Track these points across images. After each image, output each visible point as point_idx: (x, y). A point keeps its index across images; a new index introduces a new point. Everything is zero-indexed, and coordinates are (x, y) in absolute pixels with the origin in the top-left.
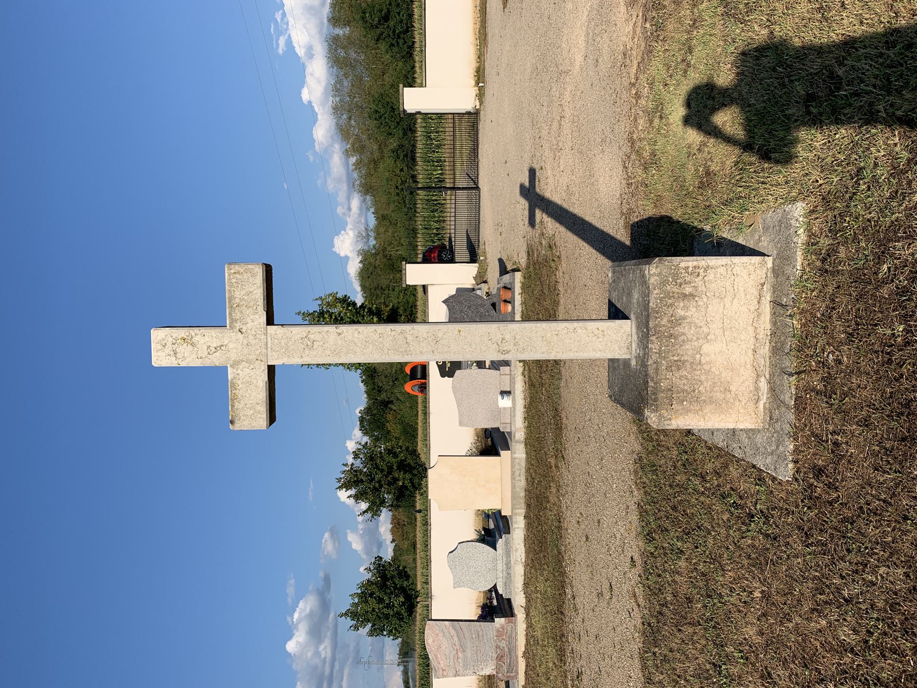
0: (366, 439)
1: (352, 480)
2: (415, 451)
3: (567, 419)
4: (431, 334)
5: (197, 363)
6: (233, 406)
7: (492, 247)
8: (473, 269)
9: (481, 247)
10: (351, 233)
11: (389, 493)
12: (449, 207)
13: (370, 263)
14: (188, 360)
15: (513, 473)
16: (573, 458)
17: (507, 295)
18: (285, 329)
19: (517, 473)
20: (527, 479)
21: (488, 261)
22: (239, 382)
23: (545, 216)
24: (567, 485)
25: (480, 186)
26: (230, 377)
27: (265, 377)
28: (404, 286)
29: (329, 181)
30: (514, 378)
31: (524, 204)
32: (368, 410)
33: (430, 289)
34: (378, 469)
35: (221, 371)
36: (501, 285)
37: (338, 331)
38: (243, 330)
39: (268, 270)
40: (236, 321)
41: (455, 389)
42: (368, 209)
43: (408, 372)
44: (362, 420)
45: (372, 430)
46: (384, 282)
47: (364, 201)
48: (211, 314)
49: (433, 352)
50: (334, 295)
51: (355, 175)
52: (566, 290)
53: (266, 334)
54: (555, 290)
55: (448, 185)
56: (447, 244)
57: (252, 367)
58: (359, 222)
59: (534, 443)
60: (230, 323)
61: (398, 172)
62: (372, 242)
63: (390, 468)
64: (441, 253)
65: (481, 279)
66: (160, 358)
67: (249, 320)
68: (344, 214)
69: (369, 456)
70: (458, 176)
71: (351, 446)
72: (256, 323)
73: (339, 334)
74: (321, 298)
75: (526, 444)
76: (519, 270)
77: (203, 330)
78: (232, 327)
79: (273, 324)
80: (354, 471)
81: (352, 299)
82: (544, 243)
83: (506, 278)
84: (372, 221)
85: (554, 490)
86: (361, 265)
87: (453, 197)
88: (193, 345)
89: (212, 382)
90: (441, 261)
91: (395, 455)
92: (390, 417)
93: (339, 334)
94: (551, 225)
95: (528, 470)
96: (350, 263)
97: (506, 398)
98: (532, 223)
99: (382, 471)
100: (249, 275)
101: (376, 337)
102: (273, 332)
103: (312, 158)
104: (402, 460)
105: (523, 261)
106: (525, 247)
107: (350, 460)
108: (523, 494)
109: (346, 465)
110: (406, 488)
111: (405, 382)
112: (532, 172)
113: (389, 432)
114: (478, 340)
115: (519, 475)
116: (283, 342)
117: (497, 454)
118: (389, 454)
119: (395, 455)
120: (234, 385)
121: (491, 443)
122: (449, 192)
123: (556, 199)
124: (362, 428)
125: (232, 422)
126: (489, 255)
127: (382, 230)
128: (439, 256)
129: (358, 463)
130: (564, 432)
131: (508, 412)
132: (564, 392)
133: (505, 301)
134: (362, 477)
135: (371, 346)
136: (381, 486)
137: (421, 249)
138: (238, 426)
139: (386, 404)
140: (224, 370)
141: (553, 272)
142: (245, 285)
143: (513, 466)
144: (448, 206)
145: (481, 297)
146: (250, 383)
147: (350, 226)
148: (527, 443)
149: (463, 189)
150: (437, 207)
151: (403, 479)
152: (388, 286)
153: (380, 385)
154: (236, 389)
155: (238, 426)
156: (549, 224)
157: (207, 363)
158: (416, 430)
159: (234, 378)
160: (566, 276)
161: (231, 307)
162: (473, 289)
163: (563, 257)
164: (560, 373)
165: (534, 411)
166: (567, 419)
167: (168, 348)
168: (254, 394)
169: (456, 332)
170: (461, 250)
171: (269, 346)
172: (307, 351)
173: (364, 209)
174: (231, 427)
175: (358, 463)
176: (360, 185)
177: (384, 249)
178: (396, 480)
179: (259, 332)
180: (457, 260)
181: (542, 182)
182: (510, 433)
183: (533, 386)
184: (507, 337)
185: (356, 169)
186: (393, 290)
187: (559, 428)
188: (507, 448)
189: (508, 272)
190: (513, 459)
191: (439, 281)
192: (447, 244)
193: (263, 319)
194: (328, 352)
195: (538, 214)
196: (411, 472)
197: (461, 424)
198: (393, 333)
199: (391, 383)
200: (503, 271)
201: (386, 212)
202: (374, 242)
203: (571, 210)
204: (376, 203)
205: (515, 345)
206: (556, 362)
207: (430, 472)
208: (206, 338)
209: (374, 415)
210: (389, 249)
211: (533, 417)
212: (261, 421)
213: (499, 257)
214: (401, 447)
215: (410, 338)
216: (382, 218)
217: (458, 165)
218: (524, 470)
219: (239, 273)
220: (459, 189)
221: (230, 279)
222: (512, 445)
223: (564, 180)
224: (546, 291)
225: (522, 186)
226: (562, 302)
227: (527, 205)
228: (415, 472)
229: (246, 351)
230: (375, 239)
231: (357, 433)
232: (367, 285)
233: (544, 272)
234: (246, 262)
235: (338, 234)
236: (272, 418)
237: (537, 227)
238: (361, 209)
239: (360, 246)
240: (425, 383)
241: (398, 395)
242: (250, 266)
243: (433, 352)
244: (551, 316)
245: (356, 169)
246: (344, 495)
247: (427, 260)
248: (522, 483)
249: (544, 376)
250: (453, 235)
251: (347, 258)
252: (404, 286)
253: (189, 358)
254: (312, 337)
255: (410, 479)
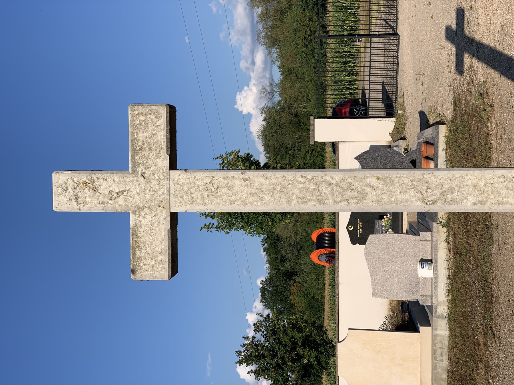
0: (267, 312)
1: (253, 355)
2: (322, 327)
3: (499, 290)
4: (345, 181)
5: (99, 209)
6: (134, 255)
7: (412, 98)
8: (389, 124)
9: (400, 100)
10: (255, 89)
11: (292, 371)
12: (364, 57)
13: (274, 122)
14: (89, 205)
15: (434, 352)
16: (506, 334)
17: (429, 151)
18: (188, 174)
19: (439, 352)
20: (450, 359)
21: (407, 114)
22: (141, 230)
23: (475, 61)
24: (498, 366)
25: (399, 32)
26: (132, 224)
27: (167, 225)
28: (312, 143)
29: (232, 33)
30: (436, 245)
31: (450, 48)
32: (269, 282)
33: (341, 146)
34: (281, 343)
35: (123, 218)
36: (422, 139)
37: (245, 177)
38: (146, 175)
39: (172, 112)
40: (138, 164)
41: (367, 254)
42: (273, 63)
43: (315, 239)
44: (263, 291)
45: (275, 303)
46: (289, 142)
47: (269, 54)
48: (112, 156)
49: (348, 201)
50: (235, 153)
51: (260, 27)
52: (500, 144)
53: (169, 179)
54: (486, 143)
55: (362, 32)
56: (359, 97)
57: (154, 213)
58: (264, 77)
59: (458, 318)
60: (133, 167)
61: (307, 22)
62: (277, 98)
63: (294, 345)
64: (353, 108)
65: (398, 134)
66: (61, 203)
67: (151, 164)
68: (247, 69)
69: (269, 327)
70: (373, 22)
71: (252, 318)
72: (159, 167)
73: (245, 180)
74: (222, 156)
75: (449, 320)
76: (442, 123)
77: (105, 174)
78: (134, 172)
79: (176, 169)
80: (255, 345)
81: (255, 157)
82: (473, 91)
83: (429, 132)
84: (278, 76)
85: (482, 372)
86: (264, 123)
87: (369, 45)
88: (95, 189)
89: (112, 229)
90: (352, 116)
91: (300, 330)
92: (294, 289)
93: (245, 180)
94: (482, 71)
95: (451, 349)
96: (253, 121)
97: (426, 267)
98: (459, 69)
99: (285, 346)
100: (153, 116)
101: (285, 184)
102: (176, 177)
103: (214, 9)
104: (307, 336)
105: (448, 113)
106: (451, 97)
107: (251, 333)
108: (445, 376)
109: (246, 338)
110: (311, 366)
111: (311, 251)
112: (460, 13)
113: (292, 306)
114: (398, 191)
115: (441, 355)
116: (186, 188)
117: (416, 330)
118: (293, 329)
119: (300, 330)
120: (136, 233)
121: (408, 317)
122: (363, 40)
123: (488, 40)
124: (264, 300)
125: (133, 272)
126: (408, 109)
127: (288, 85)
128: (351, 110)
129: (259, 336)
130: (495, 305)
131: (429, 283)
132: (496, 260)
133: (427, 158)
134: (262, 352)
135: (279, 194)
136: (284, 363)
137: (330, 105)
138: (140, 276)
139: (290, 275)
140: (125, 216)
141: (484, 123)
142: (149, 127)
143: (434, 344)
144: (362, 55)
145: (399, 153)
146: (152, 231)
147: (253, 81)
148: (450, 319)
149: (380, 35)
150: (349, 59)
151: (308, 356)
152: (293, 146)
153: (283, 253)
154: (138, 237)
155: (140, 276)
156: (480, 70)
157: (109, 208)
158: (323, 304)
159: (136, 225)
160: (500, 127)
161: (134, 150)
162: (389, 147)
163: (496, 106)
164: (491, 238)
165: (459, 282)
166: (499, 290)
167: (70, 193)
168: (156, 242)
169: (374, 179)
170: (376, 102)
171: (172, 191)
172: (211, 198)
173: (269, 62)
174: (132, 277)
175: (259, 336)
176: (267, 37)
177: (290, 106)
178: (300, 357)
179: (161, 177)
180: (371, 114)
181: (472, 23)
182: (431, 307)
183: (458, 254)
184: (433, 185)
185: (262, 20)
186: (299, 150)
187: (489, 301)
188: (427, 323)
189: (431, 126)
190: (434, 337)
191: (352, 136)
192: (359, 97)
193: (166, 163)
194: (233, 200)
195: (467, 59)
196: (317, 349)
197: (374, 294)
198: (304, 180)
199: (296, 252)
200: (425, 124)
201: (293, 65)
202: (279, 98)
203: (506, 52)
204: (281, 56)
205: (442, 194)
206: (488, 215)
207: (341, 349)
208: (109, 183)
209: (277, 286)
210: (295, 105)
211: (458, 289)
212: (162, 272)
213: (420, 109)
214: (306, 322)
215: (322, 186)
216: (288, 72)
217: (374, 12)
218: (446, 349)
219: (142, 114)
220: (375, 35)
221: (133, 121)
222: (434, 320)
223: (498, 20)
224: (476, 146)
225: (448, 29)
226: (494, 157)
227: (454, 49)
228: (321, 349)
229: (148, 196)
230: (281, 94)
231: (259, 306)
232: (271, 144)
233: (473, 123)
234: (151, 103)
235: (240, 90)
236: (174, 270)
237: (465, 74)
238: (265, 62)
239: (264, 103)
240: (334, 253)
241: (304, 267)
242: (154, 107)
243: (348, 201)
244: (484, 162)
245: (262, 20)
246: (244, 371)
247: (337, 115)
248: (444, 363)
249: (473, 242)
250: (367, 92)
251: (249, 116)
252: (312, 143)
253: (91, 203)
254: (216, 182)
255: (316, 357)
